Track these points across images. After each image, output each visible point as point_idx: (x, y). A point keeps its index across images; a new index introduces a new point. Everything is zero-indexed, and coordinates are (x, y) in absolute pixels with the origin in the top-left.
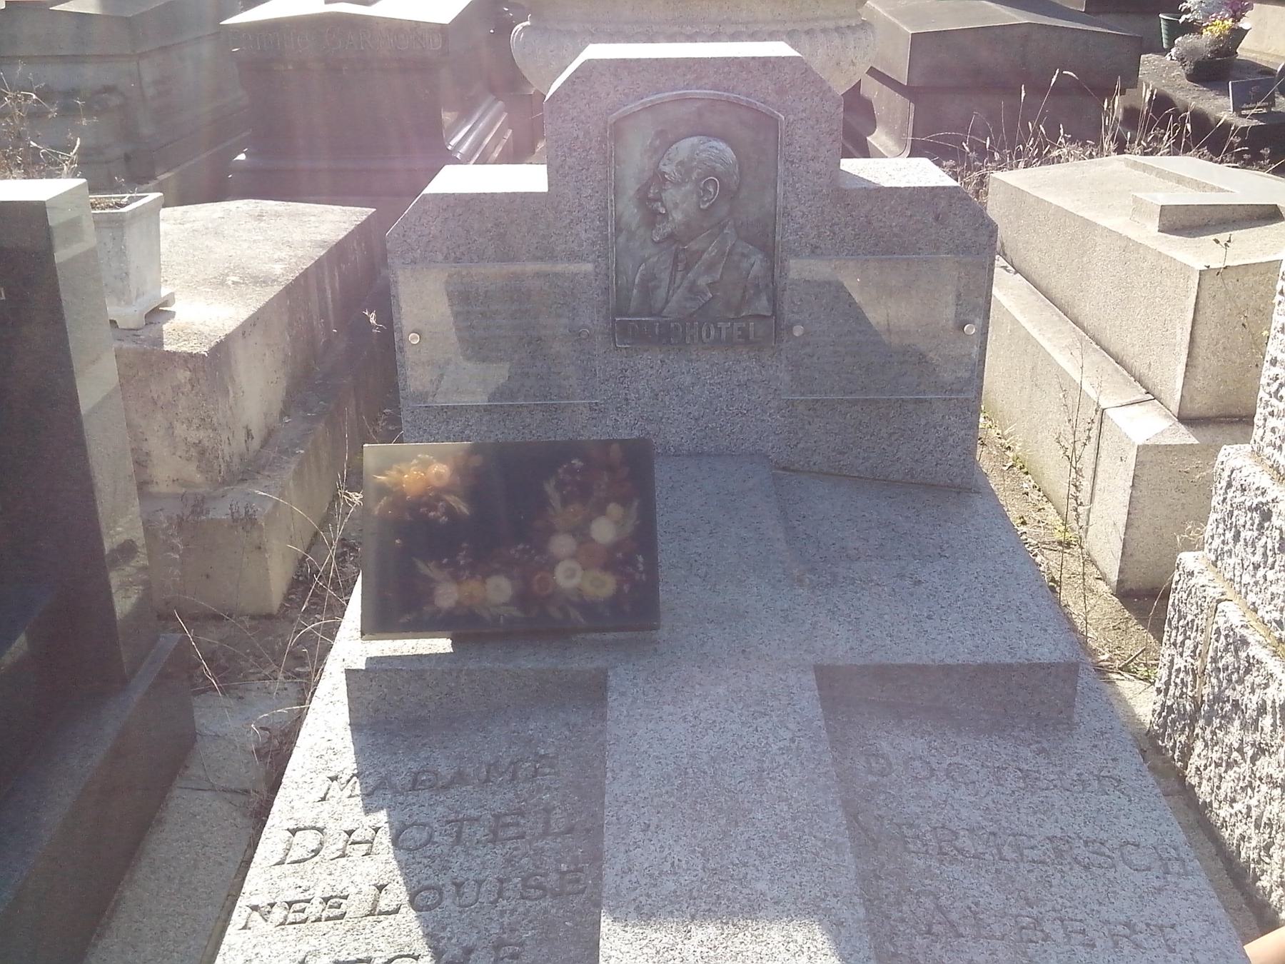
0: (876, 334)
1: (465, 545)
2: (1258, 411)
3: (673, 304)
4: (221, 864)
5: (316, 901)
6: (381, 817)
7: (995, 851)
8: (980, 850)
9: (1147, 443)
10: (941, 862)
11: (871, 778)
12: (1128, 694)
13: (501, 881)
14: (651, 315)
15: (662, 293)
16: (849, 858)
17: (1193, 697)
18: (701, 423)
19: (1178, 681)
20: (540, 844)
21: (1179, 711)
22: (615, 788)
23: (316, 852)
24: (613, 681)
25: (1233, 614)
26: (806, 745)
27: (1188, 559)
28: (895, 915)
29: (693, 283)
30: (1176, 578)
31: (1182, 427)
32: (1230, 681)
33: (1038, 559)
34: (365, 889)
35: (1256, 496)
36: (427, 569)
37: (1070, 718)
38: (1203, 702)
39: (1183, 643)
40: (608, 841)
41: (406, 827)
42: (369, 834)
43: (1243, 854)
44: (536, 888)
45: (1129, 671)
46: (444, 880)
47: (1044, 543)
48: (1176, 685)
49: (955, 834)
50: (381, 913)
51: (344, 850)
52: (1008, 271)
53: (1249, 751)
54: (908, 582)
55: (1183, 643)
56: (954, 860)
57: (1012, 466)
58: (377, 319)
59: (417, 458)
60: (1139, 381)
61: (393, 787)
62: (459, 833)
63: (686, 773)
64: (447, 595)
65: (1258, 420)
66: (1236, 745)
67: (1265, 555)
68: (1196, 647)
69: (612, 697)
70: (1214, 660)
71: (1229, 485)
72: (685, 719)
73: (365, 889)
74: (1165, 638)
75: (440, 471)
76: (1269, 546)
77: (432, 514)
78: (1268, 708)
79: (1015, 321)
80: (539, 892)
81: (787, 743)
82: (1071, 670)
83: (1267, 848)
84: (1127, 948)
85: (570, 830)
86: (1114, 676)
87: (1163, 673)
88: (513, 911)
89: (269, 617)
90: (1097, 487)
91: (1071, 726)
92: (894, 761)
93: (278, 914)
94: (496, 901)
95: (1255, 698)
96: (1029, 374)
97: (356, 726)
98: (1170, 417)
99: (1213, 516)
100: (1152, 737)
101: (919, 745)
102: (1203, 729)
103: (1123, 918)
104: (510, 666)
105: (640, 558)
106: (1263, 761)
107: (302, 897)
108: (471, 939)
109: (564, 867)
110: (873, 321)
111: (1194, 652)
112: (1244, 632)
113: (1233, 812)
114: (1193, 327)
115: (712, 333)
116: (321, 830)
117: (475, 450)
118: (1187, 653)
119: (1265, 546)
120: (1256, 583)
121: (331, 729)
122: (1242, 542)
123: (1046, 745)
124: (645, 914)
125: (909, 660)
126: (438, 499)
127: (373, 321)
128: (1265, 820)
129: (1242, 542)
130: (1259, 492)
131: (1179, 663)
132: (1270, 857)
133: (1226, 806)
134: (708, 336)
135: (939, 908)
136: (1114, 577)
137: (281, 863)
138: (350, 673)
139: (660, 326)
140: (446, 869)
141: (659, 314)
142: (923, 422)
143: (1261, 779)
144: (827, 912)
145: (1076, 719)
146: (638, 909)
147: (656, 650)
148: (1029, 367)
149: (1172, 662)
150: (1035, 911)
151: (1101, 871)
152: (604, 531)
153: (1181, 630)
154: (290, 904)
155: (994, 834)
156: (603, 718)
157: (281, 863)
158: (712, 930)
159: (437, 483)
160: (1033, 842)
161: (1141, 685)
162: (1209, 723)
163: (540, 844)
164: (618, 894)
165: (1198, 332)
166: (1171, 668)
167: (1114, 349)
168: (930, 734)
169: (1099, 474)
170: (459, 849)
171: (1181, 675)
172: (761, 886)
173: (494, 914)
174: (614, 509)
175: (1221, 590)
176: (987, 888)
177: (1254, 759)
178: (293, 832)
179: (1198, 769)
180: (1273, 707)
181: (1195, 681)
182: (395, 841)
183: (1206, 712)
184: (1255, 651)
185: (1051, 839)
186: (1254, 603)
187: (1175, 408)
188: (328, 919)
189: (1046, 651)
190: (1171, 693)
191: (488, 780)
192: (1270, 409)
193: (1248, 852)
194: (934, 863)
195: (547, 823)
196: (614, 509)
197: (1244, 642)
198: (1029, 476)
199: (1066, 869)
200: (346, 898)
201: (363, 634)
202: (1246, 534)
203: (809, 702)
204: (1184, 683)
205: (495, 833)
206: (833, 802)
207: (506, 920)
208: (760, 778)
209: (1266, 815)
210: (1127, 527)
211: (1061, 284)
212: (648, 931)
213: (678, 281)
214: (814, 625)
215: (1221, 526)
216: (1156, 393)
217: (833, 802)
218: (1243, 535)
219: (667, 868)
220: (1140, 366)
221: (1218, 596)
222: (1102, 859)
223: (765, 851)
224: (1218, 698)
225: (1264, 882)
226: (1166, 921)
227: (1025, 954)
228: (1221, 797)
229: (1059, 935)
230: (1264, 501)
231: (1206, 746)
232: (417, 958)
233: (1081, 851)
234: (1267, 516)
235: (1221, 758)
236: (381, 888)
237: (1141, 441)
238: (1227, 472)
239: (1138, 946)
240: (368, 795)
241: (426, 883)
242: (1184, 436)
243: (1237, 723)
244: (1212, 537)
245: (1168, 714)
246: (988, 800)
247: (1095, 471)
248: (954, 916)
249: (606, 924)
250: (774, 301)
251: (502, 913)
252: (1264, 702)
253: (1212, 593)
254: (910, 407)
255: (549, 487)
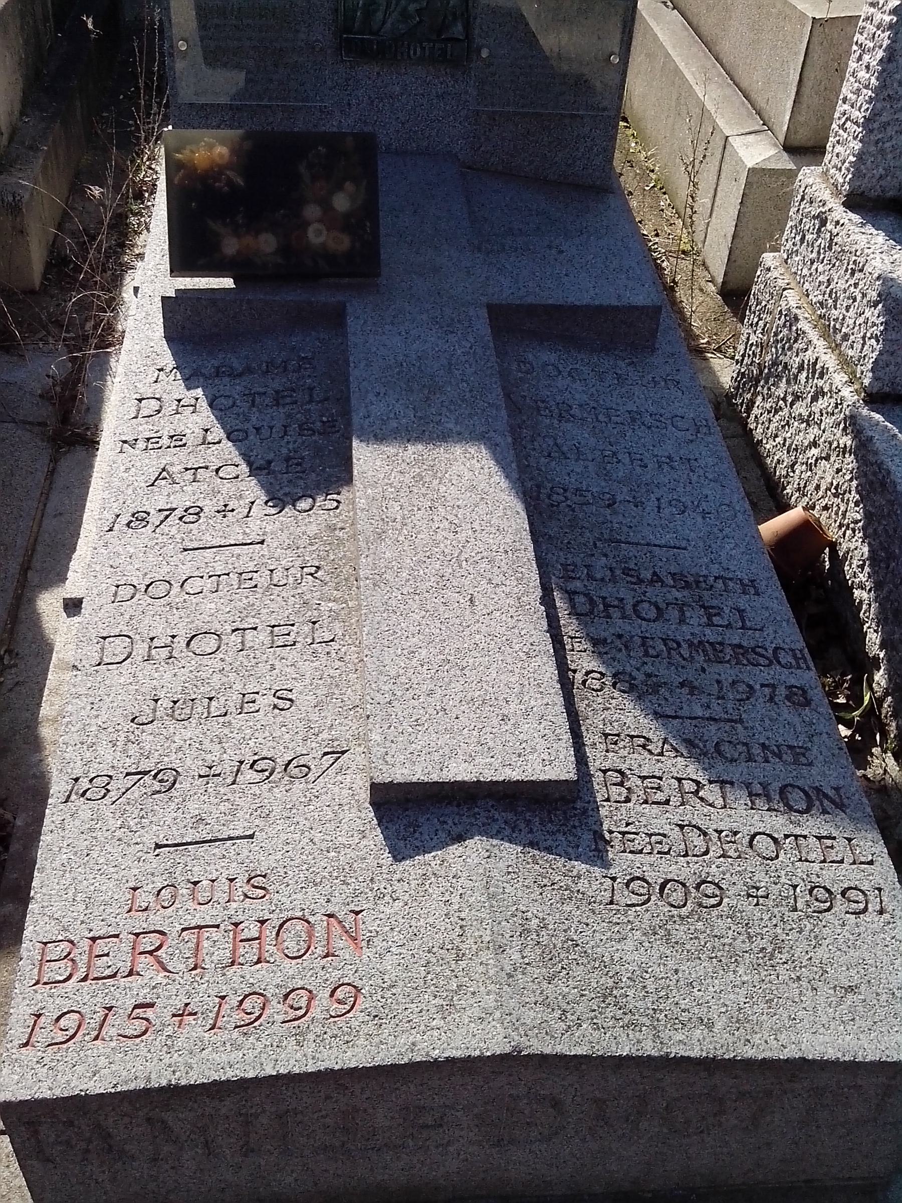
0: (547, 58)
1: (241, 209)
2: (831, 139)
3: (388, 25)
4: (32, 473)
5: (165, 438)
6: (199, 392)
7: (594, 417)
8: (585, 415)
9: (756, 166)
10: (560, 421)
11: (520, 375)
12: (717, 368)
13: (285, 427)
14: (371, 33)
15: (380, 15)
16: (504, 413)
17: (759, 364)
18: (406, 126)
19: (751, 353)
20: (308, 407)
21: (748, 375)
22: (355, 374)
23: (159, 411)
24: (350, 310)
25: (792, 299)
26: (479, 351)
27: (768, 258)
28: (529, 446)
29: (405, 9)
30: (758, 273)
31: (785, 154)
32: (783, 349)
33: (664, 264)
34: (197, 431)
35: (819, 207)
36: (215, 226)
37: (653, 345)
38: (765, 367)
39: (757, 323)
40: (353, 402)
41: (216, 398)
42: (193, 402)
43: (778, 473)
44: (308, 430)
45: (721, 351)
46: (247, 426)
47: (670, 252)
48: (749, 355)
49: (571, 407)
50: (209, 443)
51: (177, 410)
52: (667, 6)
53: (790, 399)
54: (554, 251)
55: (757, 323)
56: (568, 421)
57: (654, 187)
58: (94, 23)
59: (205, 142)
60: (759, 113)
61: (203, 375)
62: (253, 401)
63: (402, 365)
64: (231, 246)
65: (829, 147)
66: (782, 396)
67: (819, 252)
68: (765, 326)
69: (350, 320)
70: (776, 334)
71: (803, 199)
72: (400, 334)
73: (197, 431)
74: (746, 320)
75: (221, 151)
76: (822, 246)
77: (217, 184)
78: (806, 366)
79: (668, 55)
80: (310, 432)
81: (467, 350)
82: (655, 311)
83: (793, 466)
84: (666, 468)
85: (327, 399)
86: (709, 355)
87: (741, 348)
88: (295, 442)
89: (32, 292)
90: (716, 204)
91: (653, 350)
92: (535, 366)
93: (141, 445)
94: (282, 437)
95: (797, 360)
96: (673, 104)
97: (169, 337)
98: (777, 146)
99: (790, 224)
100: (729, 397)
101: (552, 357)
102: (763, 387)
103: (667, 454)
104: (277, 298)
105: (368, 224)
106: (797, 404)
107: (155, 435)
108: (271, 456)
109: (324, 419)
110: (546, 48)
111: (763, 329)
112: (798, 311)
113: (774, 444)
114: (802, 68)
115: (418, 53)
116: (158, 399)
117: (248, 136)
118: (760, 330)
119: (819, 246)
120: (811, 274)
121: (152, 340)
122: (805, 244)
123: (635, 360)
124: (379, 437)
125: (550, 302)
126: (221, 173)
127: (90, 26)
128: (794, 446)
129: (805, 244)
130: (821, 204)
131: (753, 339)
132: (794, 472)
133: (771, 442)
134: (415, 53)
135: (556, 444)
136: (720, 280)
137: (136, 417)
138: (164, 299)
139: (378, 42)
140: (248, 420)
141: (377, 33)
142: (576, 133)
143: (794, 418)
144: (489, 439)
145: (657, 346)
146: (375, 436)
147: (378, 291)
148: (674, 97)
149: (748, 339)
150: (614, 449)
151: (657, 430)
152: (341, 202)
153: (757, 313)
154: (148, 439)
155: (594, 408)
156: (345, 335)
157: (136, 417)
158: (420, 447)
159: (220, 162)
160: (619, 413)
161: (727, 362)
162: (767, 382)
163: (308, 407)
164: (362, 428)
165: (806, 73)
166: (747, 343)
167: (745, 84)
168: (560, 351)
169: (719, 194)
170: (254, 409)
171: (754, 348)
172: (451, 426)
173: (283, 443)
174: (349, 186)
175: (787, 281)
176: (586, 435)
177: (792, 404)
178: (140, 400)
179: (756, 417)
180: (808, 365)
181: (761, 351)
182: (211, 405)
183: (766, 374)
184: (803, 325)
185: (629, 412)
186: (807, 290)
187: (782, 138)
188: (175, 447)
189: (642, 296)
190: (745, 362)
191: (268, 372)
192: (837, 138)
193: (781, 471)
194: (556, 422)
195: (311, 396)
196: (349, 186)
197: (796, 319)
198: (666, 196)
199: (636, 428)
200: (184, 435)
201: (172, 271)
202: (809, 237)
203: (483, 327)
204: (754, 354)
205: (277, 400)
206: (496, 383)
207: (291, 446)
208: (450, 369)
209: (795, 442)
210: (734, 237)
211: (707, 23)
212: (382, 447)
213: (393, 6)
214: (487, 278)
215: (794, 231)
216: (770, 125)
217: (496, 383)
218: (807, 237)
219: (392, 415)
220: (761, 103)
221: (784, 285)
222: (659, 424)
223: (452, 407)
224: (775, 363)
225: (789, 490)
226: (692, 457)
227: (605, 469)
228: (768, 436)
229: (627, 461)
230: (823, 210)
231: (763, 399)
232: (237, 466)
233: (648, 420)
234: (824, 223)
235: (771, 407)
236: (206, 431)
237: (750, 165)
238: (802, 189)
239: (672, 468)
240: (187, 380)
241: (236, 428)
242: (786, 163)
243: (784, 380)
244: (787, 240)
245: (742, 379)
246: (593, 390)
247: (716, 190)
248: (565, 449)
249: (355, 443)
250: (467, 27)
251: (288, 442)
252: (803, 361)
253: (781, 283)
254: (567, 121)
255: (302, 169)
